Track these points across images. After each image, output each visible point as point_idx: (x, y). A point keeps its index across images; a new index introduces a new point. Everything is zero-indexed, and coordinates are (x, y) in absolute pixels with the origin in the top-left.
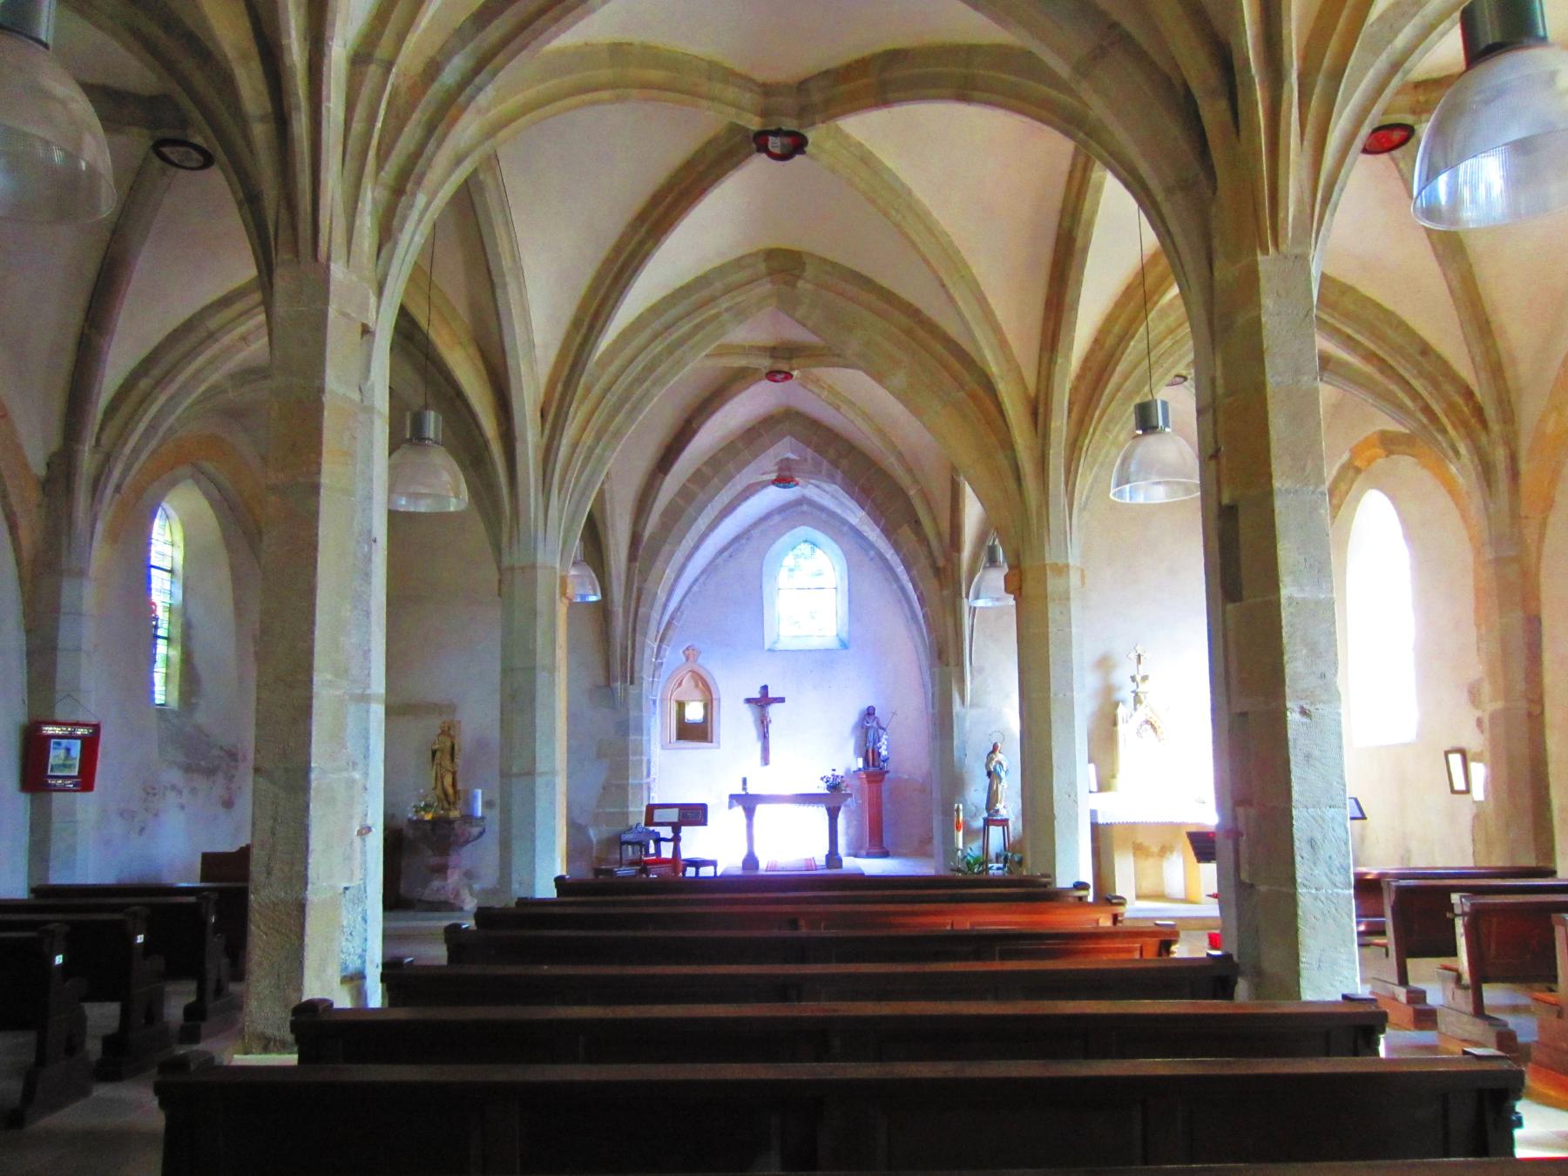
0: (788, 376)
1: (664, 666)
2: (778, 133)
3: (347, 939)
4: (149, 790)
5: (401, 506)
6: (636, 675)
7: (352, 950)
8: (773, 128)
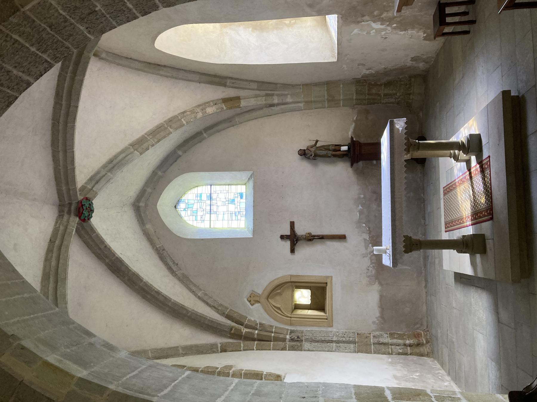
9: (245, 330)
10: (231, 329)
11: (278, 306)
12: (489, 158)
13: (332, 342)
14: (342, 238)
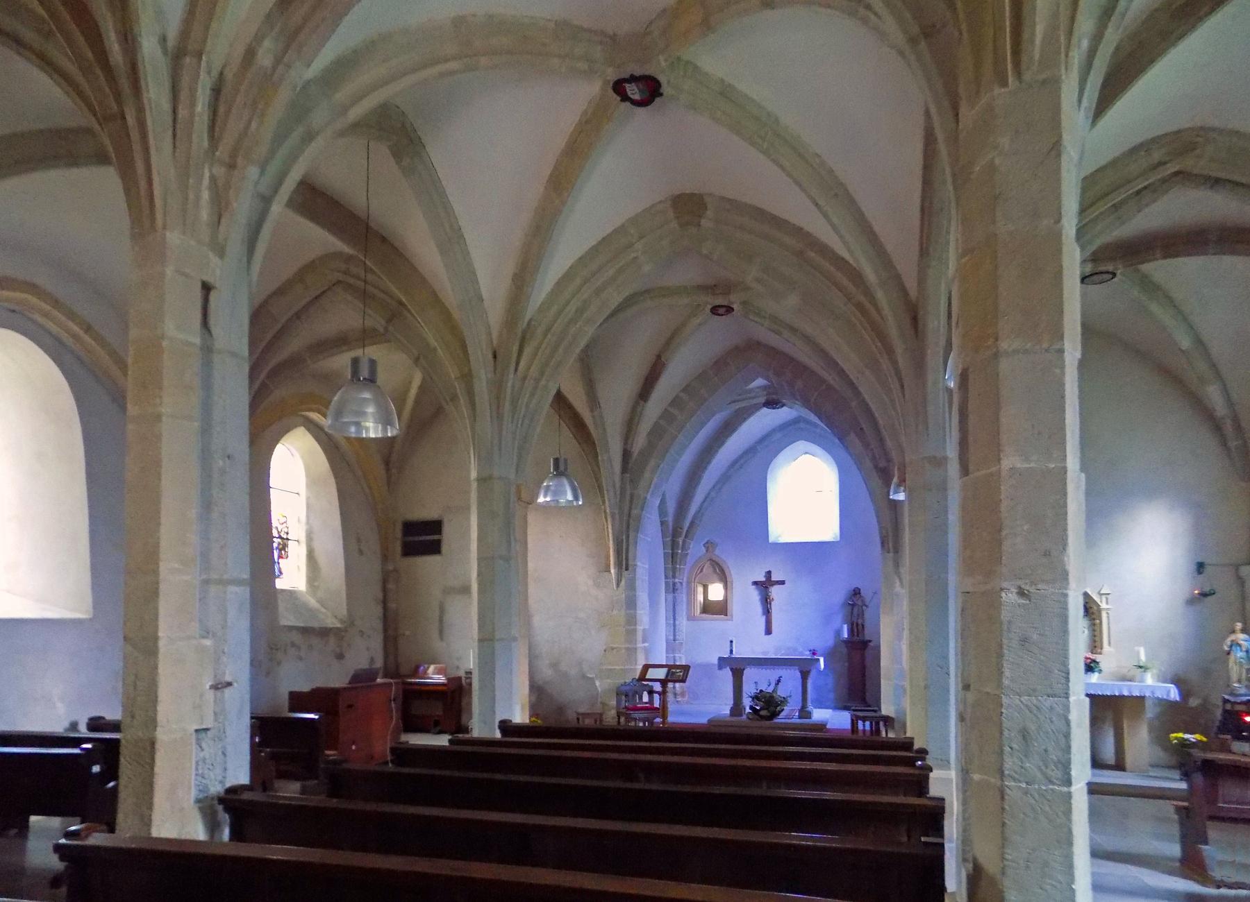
0: (729, 310)
1: (689, 557)
2: (633, 79)
3: (209, 769)
4: (273, 647)
5: (351, 433)
6: (630, 563)
7: (213, 777)
8: (627, 76)
9: (680, 540)
10: (681, 528)
11: (704, 570)
12: (1111, 276)
13: (675, 619)
14: (768, 631)
